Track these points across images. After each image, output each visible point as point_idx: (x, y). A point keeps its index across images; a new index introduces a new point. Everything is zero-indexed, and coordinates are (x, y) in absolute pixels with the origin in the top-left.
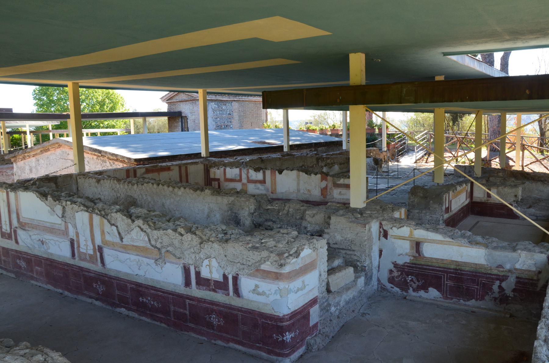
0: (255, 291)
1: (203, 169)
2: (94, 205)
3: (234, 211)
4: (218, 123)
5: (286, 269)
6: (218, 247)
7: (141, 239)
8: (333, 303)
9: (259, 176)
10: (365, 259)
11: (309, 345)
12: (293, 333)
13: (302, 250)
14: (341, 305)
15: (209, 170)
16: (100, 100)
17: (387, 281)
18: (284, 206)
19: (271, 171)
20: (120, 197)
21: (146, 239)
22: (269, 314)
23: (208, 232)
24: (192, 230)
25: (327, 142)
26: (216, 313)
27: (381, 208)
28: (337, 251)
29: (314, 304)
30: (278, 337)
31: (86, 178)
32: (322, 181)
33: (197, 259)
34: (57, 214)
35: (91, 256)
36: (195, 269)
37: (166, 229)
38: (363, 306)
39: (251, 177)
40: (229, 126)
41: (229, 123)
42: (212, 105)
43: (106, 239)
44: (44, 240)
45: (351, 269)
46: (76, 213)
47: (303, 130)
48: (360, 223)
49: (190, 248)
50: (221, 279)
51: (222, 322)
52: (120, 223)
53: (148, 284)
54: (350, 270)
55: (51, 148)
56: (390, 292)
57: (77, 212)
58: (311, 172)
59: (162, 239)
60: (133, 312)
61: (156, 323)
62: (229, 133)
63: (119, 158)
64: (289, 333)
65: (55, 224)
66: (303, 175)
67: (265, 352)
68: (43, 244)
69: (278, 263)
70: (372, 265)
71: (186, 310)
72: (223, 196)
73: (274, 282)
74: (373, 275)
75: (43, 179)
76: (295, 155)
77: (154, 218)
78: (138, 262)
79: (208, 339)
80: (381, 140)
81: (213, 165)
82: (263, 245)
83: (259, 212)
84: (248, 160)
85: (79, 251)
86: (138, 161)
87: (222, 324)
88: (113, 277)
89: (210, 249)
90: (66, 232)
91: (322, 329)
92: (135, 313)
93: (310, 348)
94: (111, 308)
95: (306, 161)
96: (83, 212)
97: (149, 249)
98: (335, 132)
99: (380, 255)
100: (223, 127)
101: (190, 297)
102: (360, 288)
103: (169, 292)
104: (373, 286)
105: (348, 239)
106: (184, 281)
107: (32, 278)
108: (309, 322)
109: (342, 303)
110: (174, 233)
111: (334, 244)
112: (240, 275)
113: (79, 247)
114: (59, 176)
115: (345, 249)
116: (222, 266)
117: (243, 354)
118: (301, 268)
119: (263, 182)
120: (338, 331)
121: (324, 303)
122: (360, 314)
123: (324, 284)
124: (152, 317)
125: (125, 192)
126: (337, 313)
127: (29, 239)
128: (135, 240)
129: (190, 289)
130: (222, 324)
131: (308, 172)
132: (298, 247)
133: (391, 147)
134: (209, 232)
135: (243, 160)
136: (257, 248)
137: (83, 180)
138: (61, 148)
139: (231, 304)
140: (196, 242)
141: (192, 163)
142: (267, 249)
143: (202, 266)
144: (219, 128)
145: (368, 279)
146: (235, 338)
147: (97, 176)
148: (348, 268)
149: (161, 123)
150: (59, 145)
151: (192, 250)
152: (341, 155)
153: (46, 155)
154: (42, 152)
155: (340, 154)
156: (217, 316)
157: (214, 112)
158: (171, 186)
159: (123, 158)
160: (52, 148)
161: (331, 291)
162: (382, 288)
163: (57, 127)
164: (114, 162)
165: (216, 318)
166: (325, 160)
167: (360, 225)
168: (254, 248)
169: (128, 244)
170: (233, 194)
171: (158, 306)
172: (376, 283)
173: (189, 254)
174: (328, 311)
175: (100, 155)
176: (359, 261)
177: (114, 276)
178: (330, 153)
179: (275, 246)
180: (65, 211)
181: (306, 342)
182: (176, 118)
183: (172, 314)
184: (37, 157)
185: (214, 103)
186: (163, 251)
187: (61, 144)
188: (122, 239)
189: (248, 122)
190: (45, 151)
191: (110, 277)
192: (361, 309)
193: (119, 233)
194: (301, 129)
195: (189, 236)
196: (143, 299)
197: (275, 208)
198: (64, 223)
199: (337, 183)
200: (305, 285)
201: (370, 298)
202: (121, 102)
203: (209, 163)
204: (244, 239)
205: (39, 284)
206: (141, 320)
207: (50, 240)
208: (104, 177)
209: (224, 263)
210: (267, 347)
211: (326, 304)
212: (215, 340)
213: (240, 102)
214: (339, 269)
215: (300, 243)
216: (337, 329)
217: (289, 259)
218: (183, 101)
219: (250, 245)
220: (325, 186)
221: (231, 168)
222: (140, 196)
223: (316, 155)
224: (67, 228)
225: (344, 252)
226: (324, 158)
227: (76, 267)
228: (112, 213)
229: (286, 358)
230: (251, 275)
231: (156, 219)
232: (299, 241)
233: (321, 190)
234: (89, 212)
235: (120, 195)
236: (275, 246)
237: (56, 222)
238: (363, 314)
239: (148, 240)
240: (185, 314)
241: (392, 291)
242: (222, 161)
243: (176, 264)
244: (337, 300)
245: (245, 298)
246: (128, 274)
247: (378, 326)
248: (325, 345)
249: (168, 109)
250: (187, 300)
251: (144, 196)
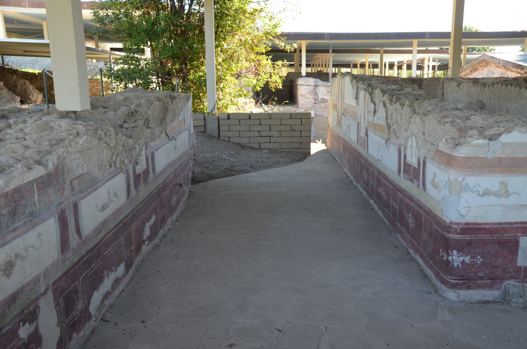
5: (461, 151)
20: (472, 102)
55: (479, 66)
64: (457, 251)
75: (407, 80)
93: (508, 298)
138: (488, 67)
160: (480, 67)
187: (488, 62)
190: (474, 71)
229: (450, 290)
251: (492, 101)
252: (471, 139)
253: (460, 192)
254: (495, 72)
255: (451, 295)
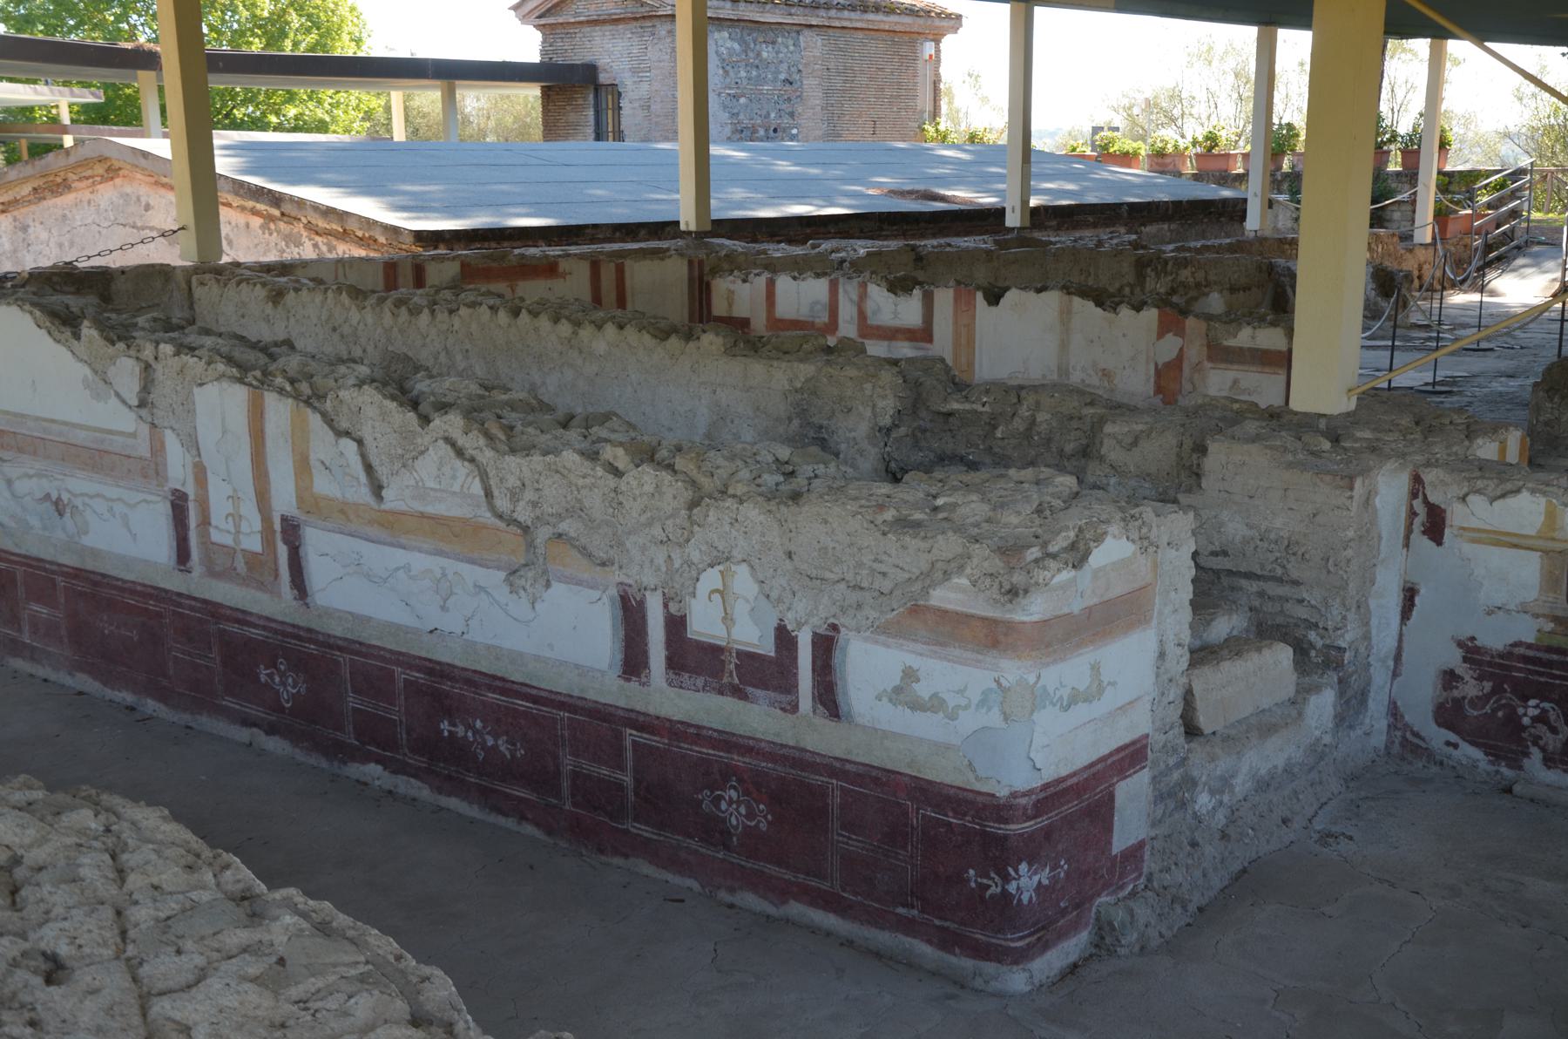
0: (902, 693)
1: (686, 277)
2: (267, 360)
3: (815, 420)
4: (741, 117)
5: (1033, 609)
6: (762, 518)
7: (456, 488)
8: (1204, 779)
9: (908, 310)
10: (1344, 618)
11: (1107, 928)
12: (1047, 870)
13: (1099, 539)
14: (1237, 789)
15: (708, 285)
16: (266, 14)
17: (1430, 716)
18: (1015, 400)
19: (955, 291)
21: (477, 488)
22: (952, 787)
23: (721, 461)
24: (657, 456)
25: (1181, 202)
26: (740, 781)
27: (1417, 423)
28: (1225, 581)
29: (1132, 765)
30: (985, 881)
31: (225, 285)
32: (1161, 335)
33: (677, 565)
34: (117, 395)
35: (252, 559)
36: (666, 606)
37: (556, 452)
38: (1327, 808)
39: (874, 313)
40: (784, 130)
41: (786, 120)
42: (720, 42)
43: (315, 490)
44: (65, 497)
45: (1282, 655)
46: (196, 390)
47: (1083, 157)
48: (1328, 472)
49: (649, 524)
50: (768, 648)
51: (765, 817)
52: (373, 427)
53: (478, 668)
54: (1282, 655)
55: (75, 177)
56: (1441, 763)
57: (201, 385)
58: (1116, 299)
59: (538, 489)
60: (412, 780)
61: (502, 821)
62: (788, 155)
63: (352, 225)
64: (1030, 864)
65: (110, 432)
66: (1084, 308)
67: (929, 942)
68: (61, 515)
69: (1000, 582)
70: (1369, 648)
71: (622, 769)
72: (770, 358)
73: (980, 657)
74: (1373, 688)
75: (55, 279)
76: (1051, 243)
77: (505, 413)
78: (439, 581)
79: (703, 887)
80: (1413, 202)
81: (726, 266)
82: (941, 516)
83: (915, 424)
84: (862, 252)
85: (206, 542)
86: (420, 236)
87: (763, 826)
88: (340, 642)
89: (727, 528)
90: (153, 467)
91: (1161, 871)
92: (419, 784)
93: (1108, 940)
94: (324, 764)
95: (1092, 270)
96: (225, 384)
97: (485, 527)
98: (1214, 165)
99: (1404, 607)
100: (762, 132)
101: (641, 719)
102: (1317, 733)
103: (559, 698)
104: (1367, 734)
105: (1272, 536)
106: (620, 657)
107: (16, 648)
108: (1111, 837)
109: (1241, 784)
110: (587, 463)
111: (1214, 554)
112: (842, 630)
113: (205, 522)
114: (116, 270)
115: (1259, 577)
116: (774, 595)
117: (842, 944)
118: (1089, 611)
119: (924, 334)
120: (1222, 890)
121: (1169, 769)
122: (1316, 836)
123: (1175, 693)
124: (488, 798)
125: (383, 340)
126: (1221, 818)
127: (7, 494)
128: (432, 493)
129: (644, 684)
130: (763, 826)
131: (1103, 299)
132: (1081, 530)
133: (1452, 228)
134: (727, 463)
135: (843, 254)
136: (918, 525)
137: (215, 289)
138: (118, 181)
139: (802, 745)
140: (675, 497)
141: (643, 254)
142: (959, 530)
143: (694, 595)
144: (742, 134)
145: (1352, 703)
146: (813, 883)
147: (269, 278)
148: (1270, 647)
149: (509, 120)
150: (110, 168)
151: (657, 531)
152: (1236, 252)
153: (56, 206)
154: (38, 194)
155: (1232, 249)
156: (747, 793)
157: (726, 72)
158: (568, 318)
159: (369, 229)
160: (80, 180)
161: (1199, 729)
162: (1407, 745)
163: (94, 116)
164: (334, 242)
165: (739, 803)
166: (1169, 267)
167: (1328, 478)
168: (904, 524)
169: (404, 508)
170: (811, 353)
171: (513, 756)
172: (1382, 724)
173: (643, 549)
174: (1183, 805)
175: (276, 213)
176: (1316, 625)
177: (340, 639)
178: (1192, 244)
179: (989, 521)
180: (153, 380)
181: (1093, 915)
182: (576, 92)
183: (566, 784)
184: (21, 213)
185: (726, 34)
186: (542, 534)
187: (117, 165)
188: (377, 489)
189: (860, 116)
190: (52, 192)
191: (329, 644)
192: (1317, 819)
193: (369, 468)
194: (1074, 150)
195: (648, 476)
196: (454, 725)
197: (980, 409)
198: (145, 429)
199: (1226, 343)
200: (1100, 683)
201: (1354, 778)
202: (351, 28)
203: (707, 255)
204: (865, 491)
205: (41, 671)
206: (442, 809)
207: (91, 497)
208: (297, 281)
209: (783, 582)
210: (937, 922)
211: (1176, 775)
212: (732, 890)
213: (830, 32)
214: (1233, 647)
215: (1087, 512)
216: (1217, 882)
217: (1044, 568)
218: (604, 22)
219: (889, 515)
220: (1174, 354)
221: (795, 278)
222: (443, 358)
223: (1135, 250)
224: (158, 449)
225: (1253, 587)
226: (1166, 262)
227: (193, 603)
228: (339, 388)
229: (1015, 968)
230: (887, 631)
231: (514, 415)
232: (1085, 507)
233: (1158, 373)
234: (250, 385)
235: (364, 351)
236: (989, 521)
237: (114, 427)
238: (1326, 837)
239: (482, 493)
240: (620, 787)
241: (1449, 757)
242: (759, 253)
243: (592, 588)
244: (1224, 764)
245: (859, 720)
246: (397, 628)
247: (1392, 885)
248: (1168, 934)
249: (543, 52)
250: (629, 731)
251: (459, 357)
252: (1046, 572)
253: (1032, 712)
254: (152, 203)
255: (1017, 980)
